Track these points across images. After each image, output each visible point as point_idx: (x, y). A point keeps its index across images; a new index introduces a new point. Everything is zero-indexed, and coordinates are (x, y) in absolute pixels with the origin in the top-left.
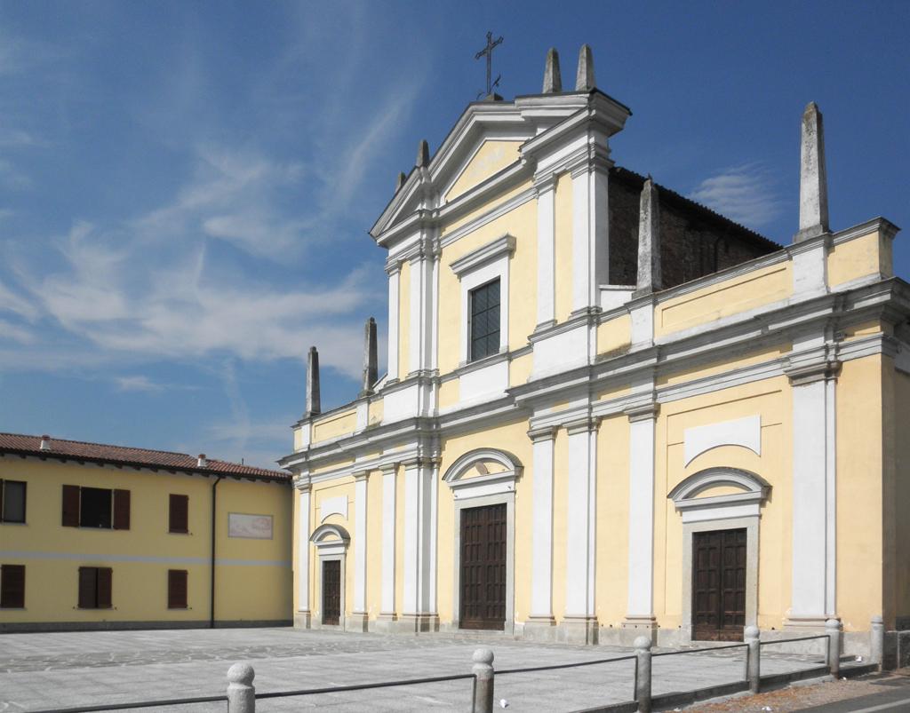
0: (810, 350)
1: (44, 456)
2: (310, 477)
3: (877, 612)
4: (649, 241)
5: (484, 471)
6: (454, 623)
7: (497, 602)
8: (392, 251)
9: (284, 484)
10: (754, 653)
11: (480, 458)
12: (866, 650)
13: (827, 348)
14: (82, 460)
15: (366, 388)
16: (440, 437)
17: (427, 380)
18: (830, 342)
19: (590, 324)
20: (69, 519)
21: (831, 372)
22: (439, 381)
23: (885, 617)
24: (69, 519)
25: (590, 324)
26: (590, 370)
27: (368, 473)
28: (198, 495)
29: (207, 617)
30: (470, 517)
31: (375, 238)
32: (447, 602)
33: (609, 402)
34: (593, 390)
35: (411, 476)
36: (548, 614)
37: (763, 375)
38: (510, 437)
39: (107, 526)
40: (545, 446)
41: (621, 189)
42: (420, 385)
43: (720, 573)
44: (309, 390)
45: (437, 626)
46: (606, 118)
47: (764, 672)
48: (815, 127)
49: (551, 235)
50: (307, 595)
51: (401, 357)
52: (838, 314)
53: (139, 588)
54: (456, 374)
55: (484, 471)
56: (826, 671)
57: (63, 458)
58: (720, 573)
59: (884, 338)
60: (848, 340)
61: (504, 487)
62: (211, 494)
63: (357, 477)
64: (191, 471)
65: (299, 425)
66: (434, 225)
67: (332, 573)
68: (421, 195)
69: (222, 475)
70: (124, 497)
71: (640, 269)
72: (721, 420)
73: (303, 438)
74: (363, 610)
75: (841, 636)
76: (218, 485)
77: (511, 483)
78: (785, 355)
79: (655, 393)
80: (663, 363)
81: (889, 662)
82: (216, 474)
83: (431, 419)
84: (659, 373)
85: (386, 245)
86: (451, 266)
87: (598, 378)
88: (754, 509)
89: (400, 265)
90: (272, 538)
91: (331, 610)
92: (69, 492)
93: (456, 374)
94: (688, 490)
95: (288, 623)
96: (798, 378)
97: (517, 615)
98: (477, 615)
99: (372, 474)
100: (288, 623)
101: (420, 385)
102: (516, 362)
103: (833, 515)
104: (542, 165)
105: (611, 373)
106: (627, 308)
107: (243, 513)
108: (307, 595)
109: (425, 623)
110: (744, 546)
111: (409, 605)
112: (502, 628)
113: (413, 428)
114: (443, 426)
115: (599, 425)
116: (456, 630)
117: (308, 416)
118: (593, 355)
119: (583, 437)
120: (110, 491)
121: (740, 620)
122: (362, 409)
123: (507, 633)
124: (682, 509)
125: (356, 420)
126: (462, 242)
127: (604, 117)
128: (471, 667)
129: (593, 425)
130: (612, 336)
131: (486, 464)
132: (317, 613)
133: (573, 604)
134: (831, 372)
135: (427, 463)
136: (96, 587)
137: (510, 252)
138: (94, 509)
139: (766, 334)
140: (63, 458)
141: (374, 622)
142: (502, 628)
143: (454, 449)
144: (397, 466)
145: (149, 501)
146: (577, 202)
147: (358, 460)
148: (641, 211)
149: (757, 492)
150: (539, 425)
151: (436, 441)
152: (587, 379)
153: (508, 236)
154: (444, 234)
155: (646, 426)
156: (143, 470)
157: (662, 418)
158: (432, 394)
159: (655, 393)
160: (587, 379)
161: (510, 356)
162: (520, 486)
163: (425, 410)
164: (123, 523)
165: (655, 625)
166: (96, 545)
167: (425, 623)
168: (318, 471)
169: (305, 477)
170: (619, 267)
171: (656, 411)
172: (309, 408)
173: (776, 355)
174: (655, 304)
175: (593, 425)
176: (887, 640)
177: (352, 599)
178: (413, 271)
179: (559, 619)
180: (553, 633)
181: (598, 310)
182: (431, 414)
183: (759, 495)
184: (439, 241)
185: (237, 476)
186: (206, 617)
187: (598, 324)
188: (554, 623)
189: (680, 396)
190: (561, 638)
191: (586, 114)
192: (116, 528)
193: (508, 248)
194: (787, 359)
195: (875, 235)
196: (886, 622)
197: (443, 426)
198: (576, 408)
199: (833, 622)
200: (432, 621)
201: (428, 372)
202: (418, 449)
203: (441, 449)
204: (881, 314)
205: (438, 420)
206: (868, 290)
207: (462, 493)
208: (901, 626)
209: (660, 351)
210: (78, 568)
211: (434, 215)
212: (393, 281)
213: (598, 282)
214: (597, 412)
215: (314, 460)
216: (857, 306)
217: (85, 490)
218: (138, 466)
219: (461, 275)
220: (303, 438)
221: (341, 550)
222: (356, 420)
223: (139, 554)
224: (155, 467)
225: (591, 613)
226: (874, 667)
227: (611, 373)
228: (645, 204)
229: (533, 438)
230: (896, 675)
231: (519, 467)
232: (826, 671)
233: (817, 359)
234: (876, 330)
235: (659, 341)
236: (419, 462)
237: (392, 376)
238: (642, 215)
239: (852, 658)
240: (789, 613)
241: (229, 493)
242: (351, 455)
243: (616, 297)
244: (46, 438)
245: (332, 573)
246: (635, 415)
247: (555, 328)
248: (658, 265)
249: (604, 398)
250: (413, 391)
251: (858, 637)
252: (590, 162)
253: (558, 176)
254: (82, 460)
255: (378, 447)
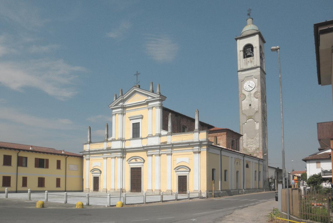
0: (196, 148)
1: (32, 151)
2: (89, 157)
3: (206, 189)
4: (170, 124)
5: (136, 160)
6: (129, 191)
7: (139, 187)
8: (114, 111)
9: (81, 157)
10: (189, 194)
11: (135, 158)
12: (204, 195)
13: (199, 149)
14: (40, 152)
15: (106, 139)
16: (125, 152)
17: (123, 140)
18: (199, 148)
19: (159, 137)
20: (36, 166)
21: (199, 152)
22: (125, 141)
23: (207, 190)
24: (36, 166)
25: (159, 137)
26: (160, 146)
27: (107, 158)
28: (62, 159)
29: (15, 190)
30: (133, 169)
31: (110, 107)
32: (127, 186)
33: (163, 151)
34: (160, 149)
35: (119, 160)
36: (114, 188)
37: (189, 151)
38: (143, 154)
39: (43, 167)
40: (150, 158)
41: (165, 112)
42: (121, 141)
43: (183, 182)
44: (89, 136)
45: (125, 192)
46: (162, 98)
47: (190, 197)
48: (197, 113)
49: (151, 119)
50: (88, 184)
51: (116, 133)
52: (200, 144)
53: (50, 183)
54: (130, 140)
55: (136, 160)
56: (198, 197)
57: (36, 152)
58: (183, 182)
59: (207, 149)
60: (202, 148)
61: (141, 164)
62: (65, 161)
63: (104, 158)
64: (62, 155)
65: (86, 144)
66: (124, 108)
67: (96, 180)
68: (121, 101)
69: (68, 156)
70: (47, 160)
71: (169, 129)
72: (184, 157)
73: (87, 147)
74: (106, 188)
75: (201, 193)
76: (67, 158)
77: (143, 163)
78: (193, 149)
79: (171, 151)
80: (173, 146)
81: (207, 197)
82: (67, 155)
83: (124, 149)
84: (172, 148)
85: (113, 109)
86: (129, 118)
87: (162, 146)
88: (188, 173)
89: (116, 114)
90: (78, 170)
91: (96, 187)
92: (36, 159)
93: (130, 140)
94: (177, 168)
95: (82, 191)
96: (195, 153)
97: (144, 189)
98: (134, 189)
99: (108, 158)
100: (82, 191)
101: (121, 141)
102: (143, 140)
103: (200, 174)
104: (150, 104)
105: (163, 147)
106: (166, 135)
107: (72, 163)
108: (88, 184)
109: (122, 191)
110: (186, 178)
111: (119, 187)
112: (141, 192)
113: (120, 150)
114: (127, 150)
115: (161, 155)
116: (130, 192)
117: (89, 142)
118: (160, 142)
119: (158, 157)
120: (44, 159)
121: (186, 190)
122: (105, 143)
123: (142, 193)
124: (176, 172)
125: (104, 146)
126: (131, 113)
127: (162, 99)
128: (116, 203)
129: (160, 155)
130: (163, 139)
131: (137, 159)
132: (92, 188)
133: (156, 187)
134: (199, 152)
135: (123, 158)
136: (41, 182)
137: (142, 118)
138: (41, 164)
139: (190, 145)
140: (36, 152)
141: (109, 191)
142: (141, 192)
143: (129, 155)
144: (115, 157)
145: (52, 161)
146: (157, 113)
147: (104, 155)
148: (169, 118)
149: (188, 170)
150: (149, 154)
151: (124, 153)
152: (159, 147)
153: (142, 115)
154: (126, 110)
155: (170, 157)
156: (56, 155)
157: (172, 155)
158: (124, 143)
159: (171, 151)
160: (159, 147)
161: (142, 139)
162: (144, 164)
163: (122, 146)
164: (47, 167)
165: (172, 191)
166: (42, 172)
167: (122, 191)
168: (91, 156)
169: (88, 157)
170: (164, 127)
171: (171, 154)
172: (89, 140)
173: (191, 148)
174: (171, 136)
175: (160, 155)
176: (207, 193)
177: (102, 185)
178: (119, 117)
179: (153, 190)
180: (152, 193)
181: (161, 134)
182: (124, 148)
183: (189, 170)
184: (125, 111)
185: (72, 156)
186: (64, 189)
187: (161, 137)
188: (152, 191)
189: (176, 153)
190: (154, 194)
191: (159, 98)
192: (46, 168)
193: (142, 117)
194: (193, 149)
195: (206, 133)
196: (207, 191)
197: (127, 150)
198: (157, 152)
199: (199, 191)
200: (124, 190)
201: (123, 138)
202: (121, 154)
203: (126, 155)
204: (207, 145)
205: (126, 149)
206: (204, 142)
207: (131, 164)
208: (209, 191)
209: (173, 144)
210: (22, 177)
211: (124, 106)
212: (114, 117)
213: (161, 129)
214: (160, 153)
215: (90, 153)
216: (203, 143)
217: (39, 159)
218: (51, 154)
219: (130, 120)
220: (87, 147)
221: (99, 174)
222: (104, 146)
223: (50, 174)
224: (55, 154)
225: (160, 189)
226: (205, 197)
227: (163, 147)
228: (170, 117)
229: (148, 156)
230: (208, 199)
231: (144, 161)
232: (198, 197)
233: (197, 150)
234: (205, 147)
235: (172, 142)
236: (121, 157)
237: (113, 137)
238: (169, 119)
239: (203, 196)
240: (193, 189)
241: (70, 160)
242: (103, 153)
243: (164, 132)
244: (32, 147)
245: (96, 180)
246: (168, 154)
247: (152, 136)
248: (172, 128)
249: (162, 150)
250: (120, 142)
251: (203, 193)
252: (159, 107)
253: (153, 107)
254: (40, 152)
255: (111, 153)
